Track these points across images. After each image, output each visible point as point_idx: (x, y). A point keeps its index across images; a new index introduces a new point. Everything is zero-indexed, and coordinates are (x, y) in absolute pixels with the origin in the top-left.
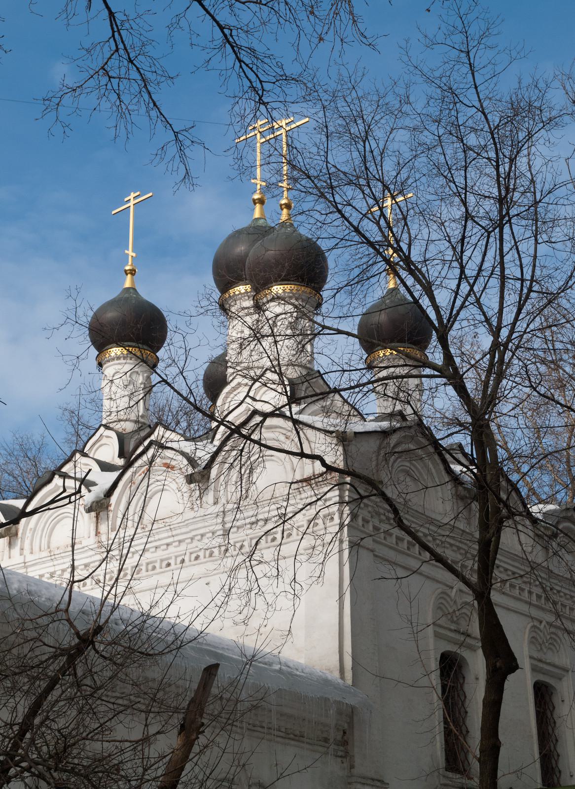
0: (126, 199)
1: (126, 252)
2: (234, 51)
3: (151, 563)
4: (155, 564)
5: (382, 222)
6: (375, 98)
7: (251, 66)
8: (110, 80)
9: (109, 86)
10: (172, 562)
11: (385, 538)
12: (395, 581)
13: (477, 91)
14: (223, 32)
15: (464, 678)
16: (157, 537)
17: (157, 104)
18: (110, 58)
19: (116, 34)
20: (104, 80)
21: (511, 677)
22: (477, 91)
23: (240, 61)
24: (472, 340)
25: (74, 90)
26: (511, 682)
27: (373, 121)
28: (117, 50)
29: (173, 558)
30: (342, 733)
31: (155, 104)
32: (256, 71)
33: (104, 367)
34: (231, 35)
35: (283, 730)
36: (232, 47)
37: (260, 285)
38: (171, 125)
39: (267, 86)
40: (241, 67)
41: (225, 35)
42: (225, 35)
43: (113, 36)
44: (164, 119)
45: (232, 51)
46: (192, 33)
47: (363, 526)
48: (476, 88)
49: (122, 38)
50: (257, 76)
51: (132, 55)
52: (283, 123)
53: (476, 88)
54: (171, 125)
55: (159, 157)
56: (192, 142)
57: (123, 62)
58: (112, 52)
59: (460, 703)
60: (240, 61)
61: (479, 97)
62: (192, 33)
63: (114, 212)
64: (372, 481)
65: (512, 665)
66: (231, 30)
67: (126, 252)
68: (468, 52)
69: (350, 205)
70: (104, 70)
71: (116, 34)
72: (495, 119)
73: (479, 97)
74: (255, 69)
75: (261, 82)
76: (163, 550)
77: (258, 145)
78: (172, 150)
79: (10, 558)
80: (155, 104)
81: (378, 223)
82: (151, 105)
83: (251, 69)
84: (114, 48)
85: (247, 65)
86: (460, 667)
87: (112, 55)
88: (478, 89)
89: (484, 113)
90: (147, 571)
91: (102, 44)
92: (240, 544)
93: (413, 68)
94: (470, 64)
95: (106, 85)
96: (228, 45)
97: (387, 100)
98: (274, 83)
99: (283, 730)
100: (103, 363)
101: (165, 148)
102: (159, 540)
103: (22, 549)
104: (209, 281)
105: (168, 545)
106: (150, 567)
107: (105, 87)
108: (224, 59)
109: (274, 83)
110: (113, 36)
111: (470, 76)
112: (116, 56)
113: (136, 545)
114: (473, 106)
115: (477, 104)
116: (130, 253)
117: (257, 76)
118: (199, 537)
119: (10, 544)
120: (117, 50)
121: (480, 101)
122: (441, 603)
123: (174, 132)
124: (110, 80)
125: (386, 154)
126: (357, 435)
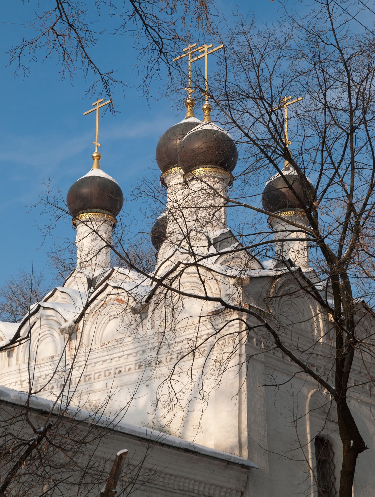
0: (93, 104)
1: (94, 142)
2: (142, 18)
3: (108, 370)
4: (111, 371)
5: (271, 125)
6: (267, 35)
7: (154, 28)
8: (57, 37)
9: (57, 42)
10: (122, 369)
11: (274, 353)
12: (275, 387)
13: (334, 33)
14: (133, 5)
15: (334, 454)
16: (94, 356)
17: (88, 55)
18: (57, 21)
19: (60, 5)
20: (54, 37)
21: (360, 455)
22: (334, 33)
23: (146, 25)
24: (331, 213)
25: (31, 43)
26: (361, 457)
27: (265, 52)
28: (61, 16)
29: (123, 367)
30: (240, 494)
31: (86, 55)
32: (158, 32)
33: (78, 227)
34: (140, 7)
35: (196, 492)
36: (140, 15)
37: (188, 170)
38: (98, 70)
39: (165, 41)
40: (147, 29)
41: (135, 8)
42: (135, 8)
43: (58, 7)
44: (93, 66)
45: (140, 18)
46: (112, 6)
47: (257, 344)
48: (334, 30)
49: (63, 9)
50: (158, 35)
51: (71, 20)
52: (205, 49)
53: (334, 30)
54: (98, 70)
55: (90, 93)
56: (114, 81)
57: (66, 25)
58: (58, 18)
59: (331, 472)
60: (146, 25)
61: (335, 37)
62: (112, 6)
63: (84, 114)
64: (264, 313)
65: (360, 446)
66: (140, 3)
67: (94, 142)
68: (328, 5)
69: (247, 112)
70: (53, 29)
71: (60, 5)
72: (348, 53)
73: (335, 37)
74: (157, 30)
75: (161, 39)
76: (108, 363)
77: (189, 64)
78: (100, 86)
79: (9, 366)
80: (86, 55)
81: (268, 126)
82: (84, 55)
83: (154, 30)
84: (59, 15)
85: (151, 27)
86: (331, 446)
87: (58, 19)
88: (336, 31)
89: (339, 50)
90: (95, 379)
91: (50, 12)
92: (98, 374)
93: (289, 18)
94: (329, 14)
95: (55, 41)
96: (137, 14)
97: (275, 36)
98: (170, 40)
99: (196, 492)
100: (77, 224)
101: (95, 85)
102: (97, 358)
103: (17, 360)
104: (155, 165)
105: (119, 357)
106: (107, 373)
107: (54, 41)
108: (135, 23)
109: (170, 40)
110: (58, 7)
111: (329, 22)
112: (60, 20)
113: (91, 359)
114: (332, 44)
115: (335, 44)
116: (97, 144)
117: (158, 35)
118: (141, 352)
119: (9, 356)
120: (61, 16)
121: (336, 40)
122: (317, 400)
123: (101, 75)
124: (57, 37)
125: (274, 76)
126: (253, 279)
